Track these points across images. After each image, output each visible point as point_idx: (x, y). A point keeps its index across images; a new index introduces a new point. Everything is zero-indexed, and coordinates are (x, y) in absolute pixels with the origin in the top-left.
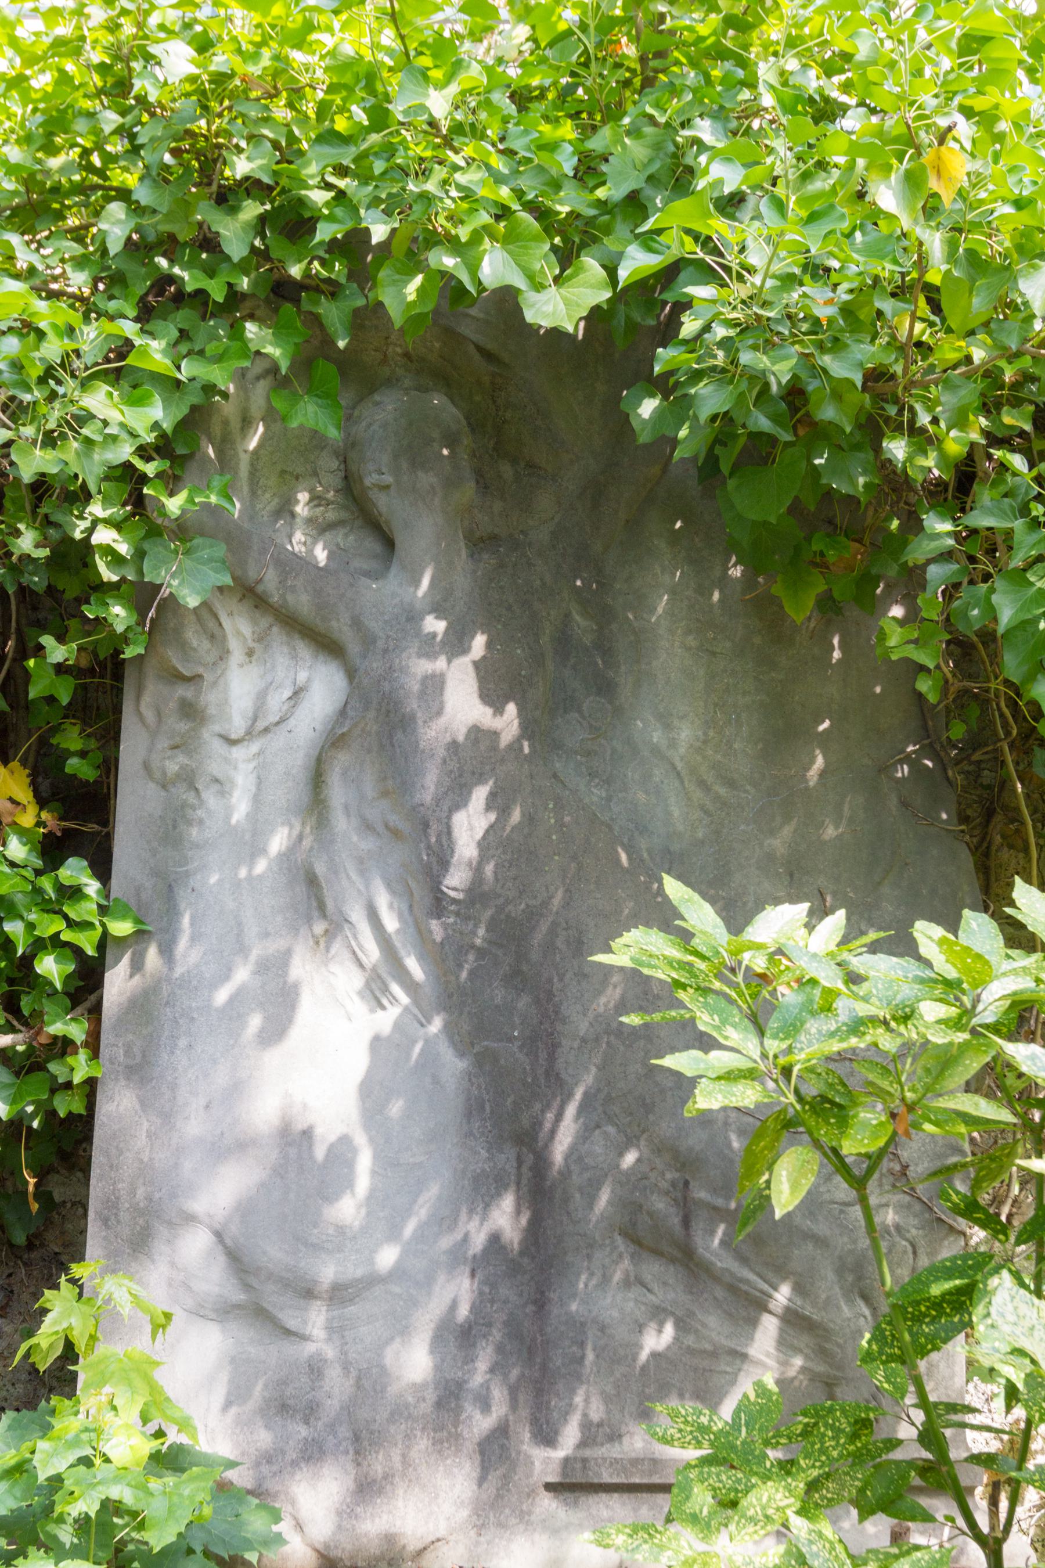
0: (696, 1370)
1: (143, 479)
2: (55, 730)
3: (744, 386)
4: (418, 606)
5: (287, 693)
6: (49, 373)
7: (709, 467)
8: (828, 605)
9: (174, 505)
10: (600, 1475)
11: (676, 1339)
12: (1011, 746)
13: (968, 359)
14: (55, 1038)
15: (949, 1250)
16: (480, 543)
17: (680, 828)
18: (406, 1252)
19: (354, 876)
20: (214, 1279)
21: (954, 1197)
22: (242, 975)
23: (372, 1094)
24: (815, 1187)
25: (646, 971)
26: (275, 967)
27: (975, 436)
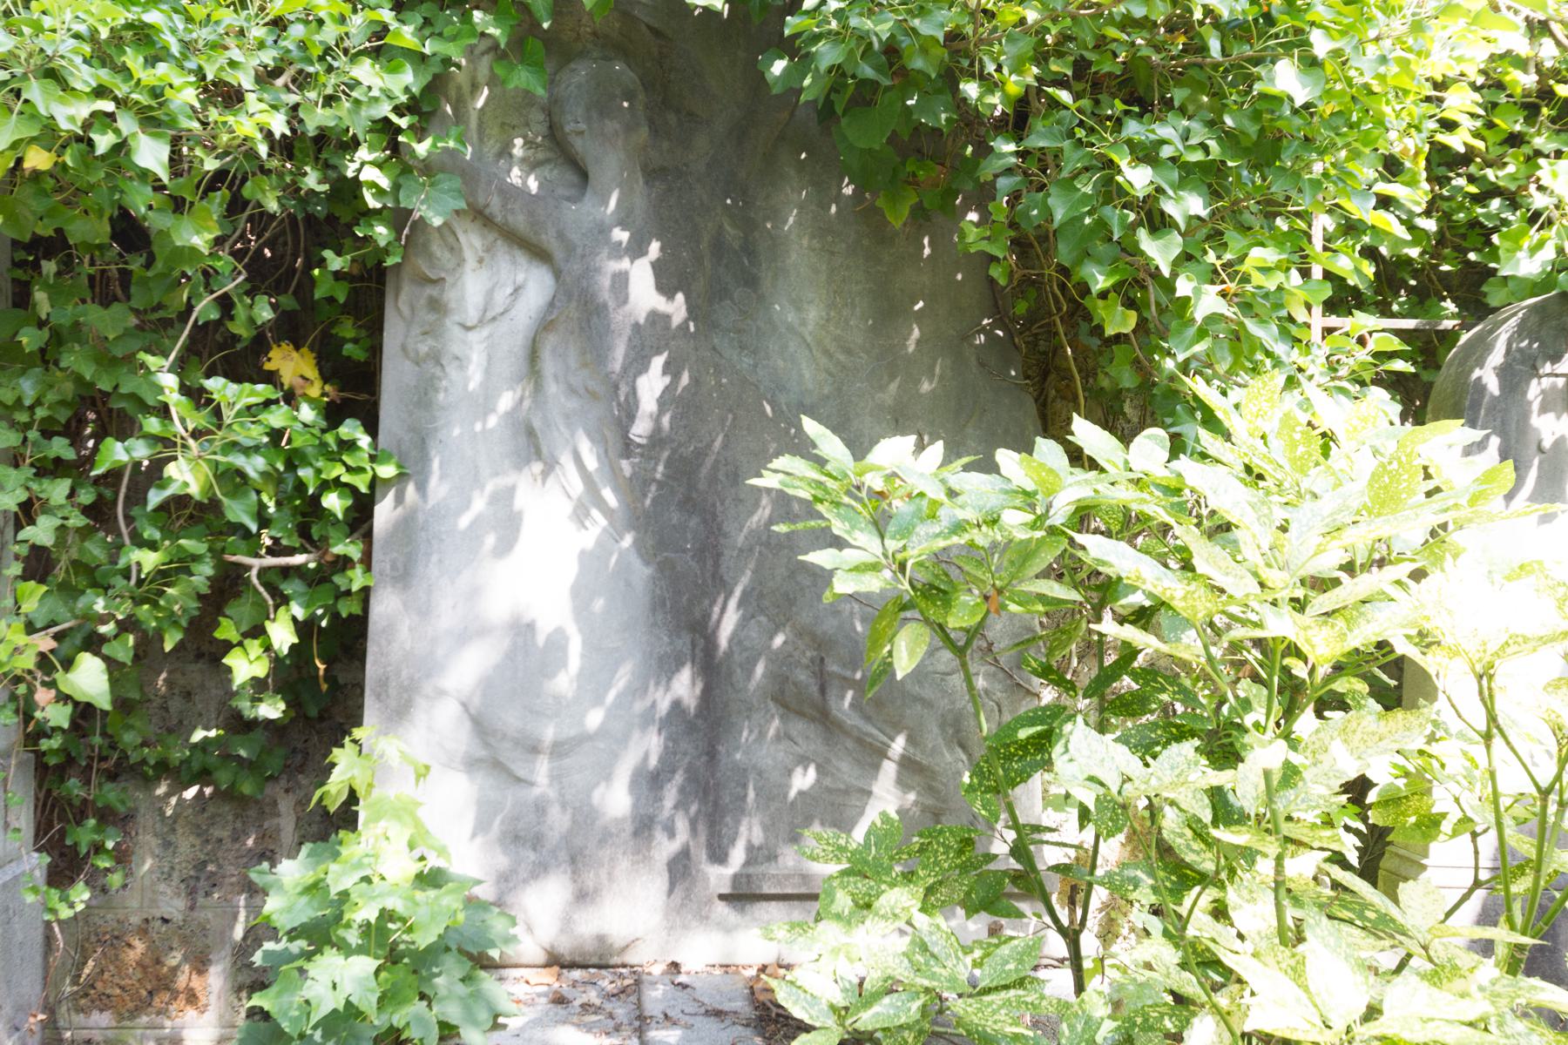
0: (833, 805)
1: (399, 130)
2: (335, 323)
3: (853, 44)
4: (607, 221)
5: (509, 290)
6: (328, 50)
7: (826, 112)
8: (920, 215)
9: (422, 149)
10: (760, 887)
11: (818, 781)
12: (1062, 319)
13: (1022, 21)
14: (338, 556)
15: (1026, 707)
16: (653, 174)
17: (810, 386)
18: (611, 717)
19: (562, 428)
20: (460, 738)
21: (1034, 664)
22: (479, 504)
23: (580, 595)
24: (922, 661)
25: (790, 491)
27: (1030, 80)
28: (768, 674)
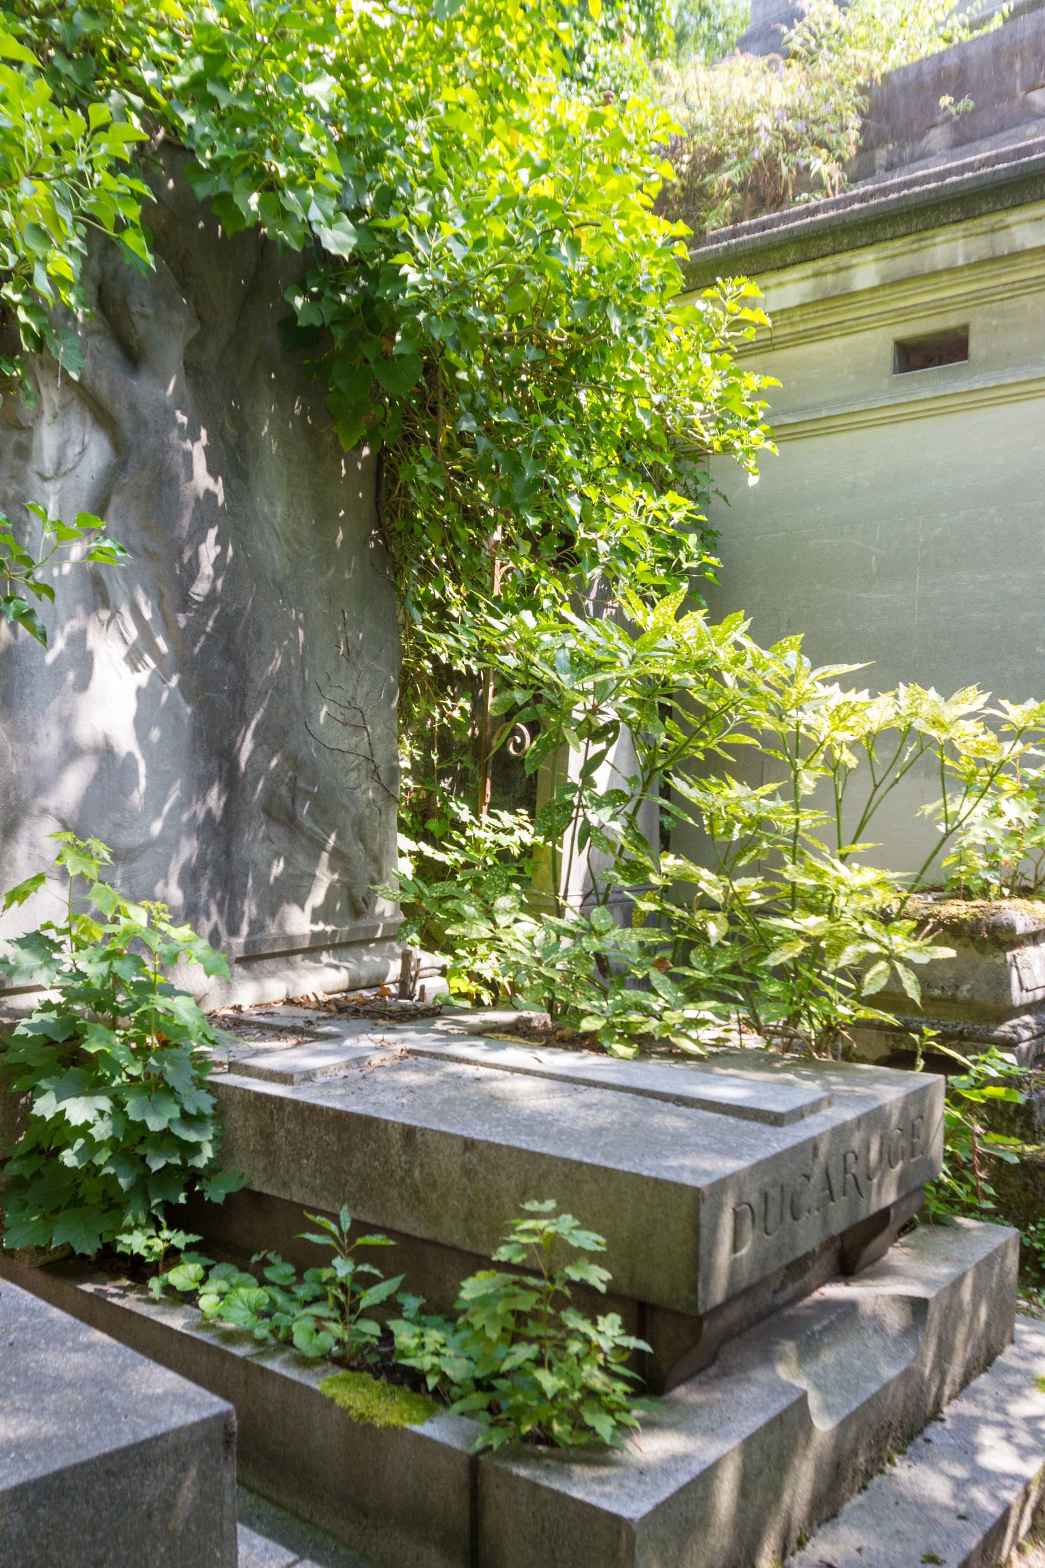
23: (141, 725)
26: (78, 639)
28: (265, 789)
